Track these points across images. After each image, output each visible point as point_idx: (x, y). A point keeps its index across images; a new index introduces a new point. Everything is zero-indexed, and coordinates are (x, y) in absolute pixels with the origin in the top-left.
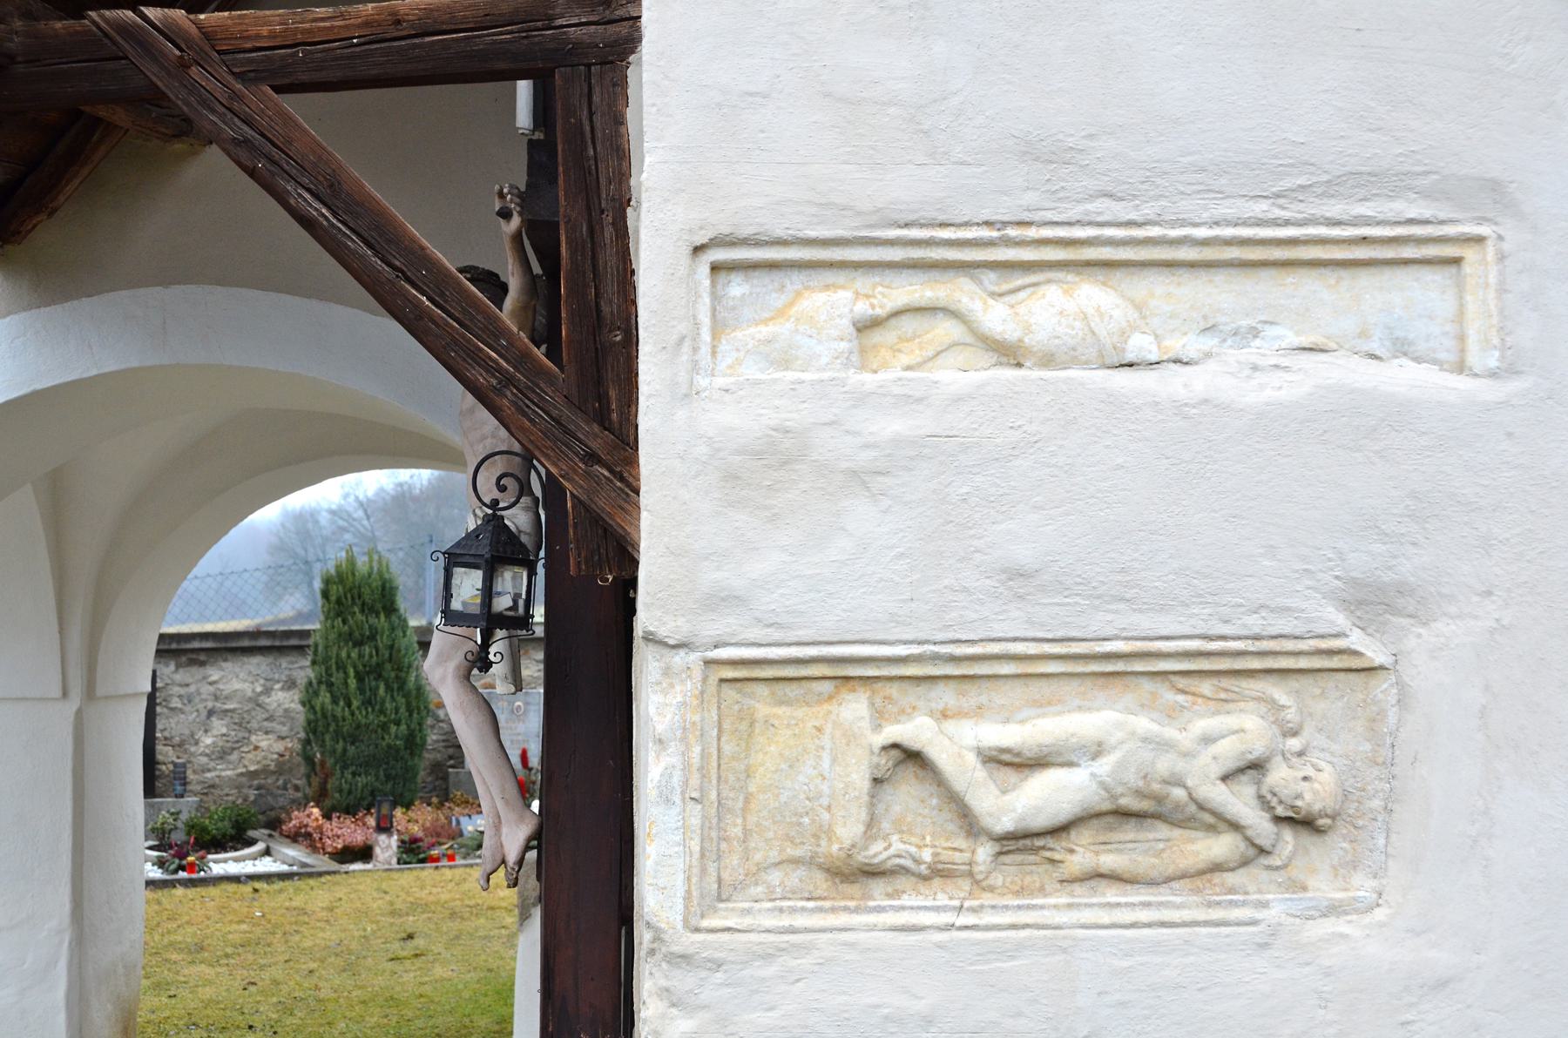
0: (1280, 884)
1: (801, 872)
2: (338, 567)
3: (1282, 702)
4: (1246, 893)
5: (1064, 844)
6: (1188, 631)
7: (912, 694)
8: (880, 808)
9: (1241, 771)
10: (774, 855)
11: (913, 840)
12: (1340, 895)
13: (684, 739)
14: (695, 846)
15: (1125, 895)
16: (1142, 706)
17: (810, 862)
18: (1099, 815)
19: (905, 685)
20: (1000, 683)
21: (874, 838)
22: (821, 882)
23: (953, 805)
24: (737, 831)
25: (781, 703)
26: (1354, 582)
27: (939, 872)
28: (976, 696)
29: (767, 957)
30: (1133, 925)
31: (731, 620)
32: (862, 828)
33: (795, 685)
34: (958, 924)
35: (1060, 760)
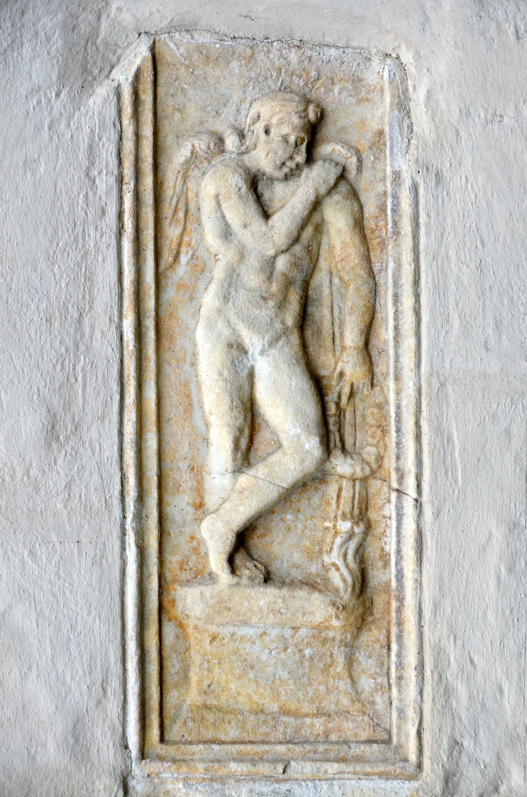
0: (376, 158)
1: (361, 656)
2: (365, 306)
3: (188, 154)
4: (385, 193)
5: (334, 383)
6: (112, 253)
7: (178, 540)
8: (296, 574)
9: (258, 198)
10: (344, 685)
11: (328, 540)
12: (388, 98)
13: (222, 780)
14: (333, 768)
15: (386, 319)
16: (191, 299)
17: (351, 648)
18: (304, 346)
19: (168, 547)
20: (166, 448)
21: (327, 580)
22: (371, 636)
23: (294, 497)
24: (319, 725)
25: (186, 677)
26: (63, 78)
27: (362, 513)
28: (180, 474)
29: (448, 693)
30: (417, 313)
31: (98, 732)
32: (316, 596)
33: (168, 663)
34: (414, 495)
35: (247, 387)
